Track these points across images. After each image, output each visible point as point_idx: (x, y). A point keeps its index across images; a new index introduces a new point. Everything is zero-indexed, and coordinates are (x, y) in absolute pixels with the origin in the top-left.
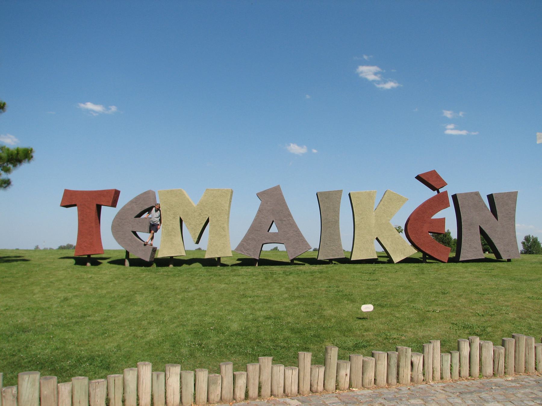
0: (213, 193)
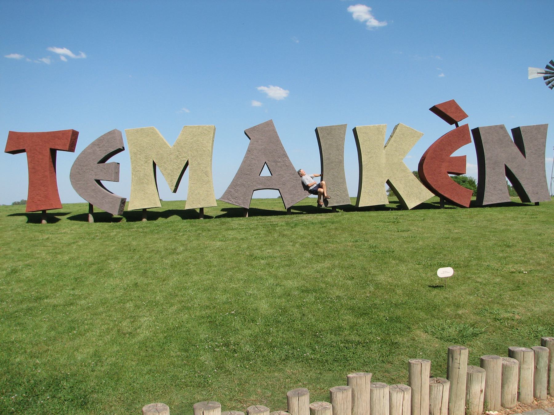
0: (192, 131)
